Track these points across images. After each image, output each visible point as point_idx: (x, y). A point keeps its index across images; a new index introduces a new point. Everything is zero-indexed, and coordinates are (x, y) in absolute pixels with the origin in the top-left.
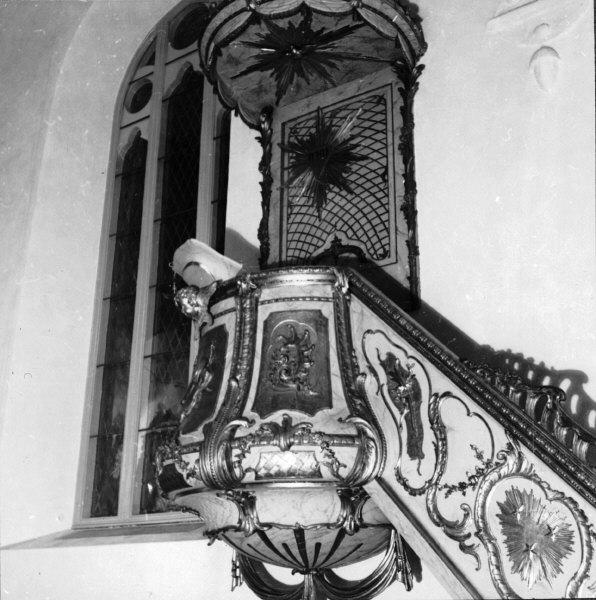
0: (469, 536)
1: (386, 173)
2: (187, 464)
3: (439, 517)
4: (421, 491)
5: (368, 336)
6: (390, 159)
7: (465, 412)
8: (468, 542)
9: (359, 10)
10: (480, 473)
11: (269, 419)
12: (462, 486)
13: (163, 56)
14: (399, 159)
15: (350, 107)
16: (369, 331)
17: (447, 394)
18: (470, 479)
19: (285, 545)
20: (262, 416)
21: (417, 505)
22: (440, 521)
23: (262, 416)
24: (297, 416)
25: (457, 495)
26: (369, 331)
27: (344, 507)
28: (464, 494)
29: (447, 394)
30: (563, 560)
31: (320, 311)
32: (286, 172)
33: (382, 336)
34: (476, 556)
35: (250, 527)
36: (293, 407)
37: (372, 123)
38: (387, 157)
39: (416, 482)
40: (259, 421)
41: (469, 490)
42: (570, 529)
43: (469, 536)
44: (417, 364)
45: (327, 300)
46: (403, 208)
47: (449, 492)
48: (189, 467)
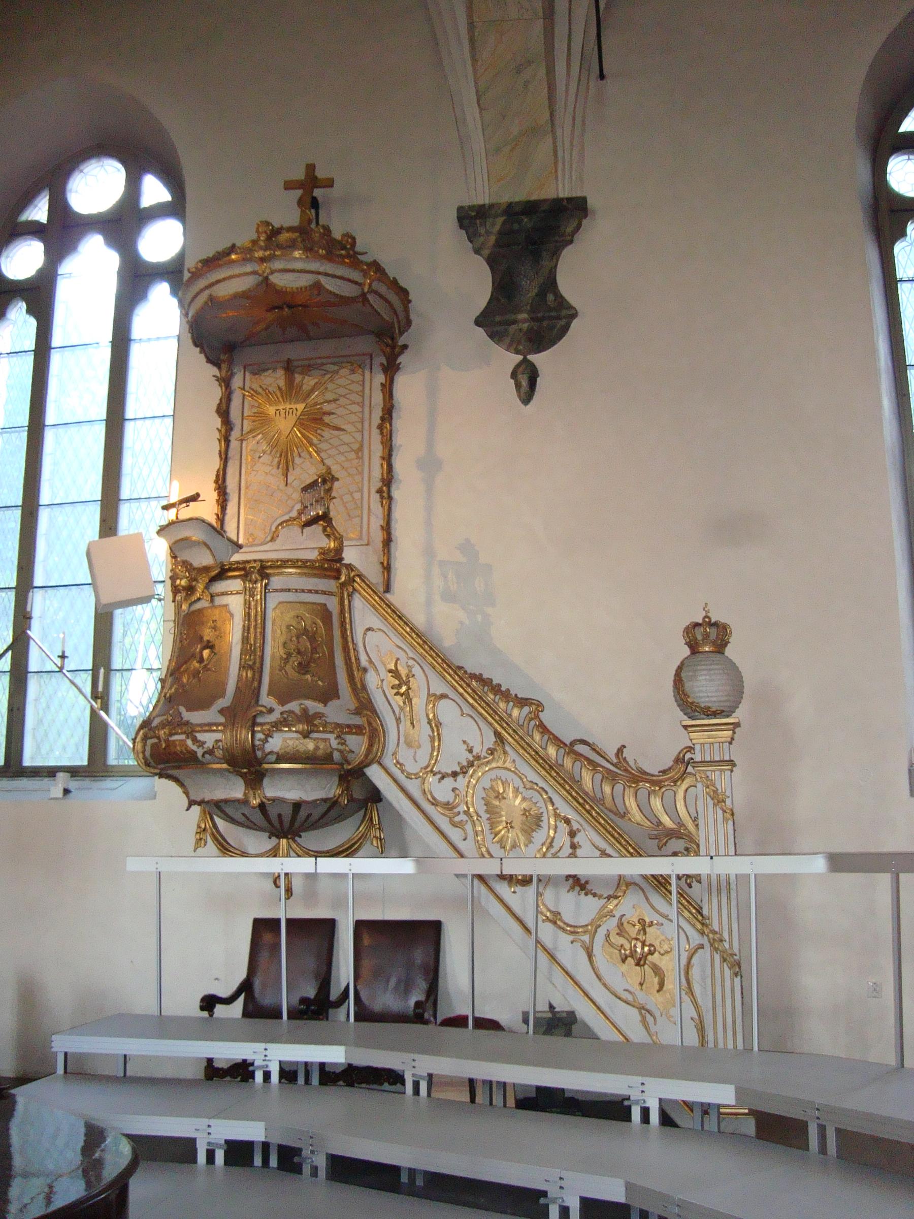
0: (459, 813)
1: (361, 449)
2: (204, 743)
3: (434, 798)
4: (417, 776)
5: (369, 633)
6: (366, 434)
7: (460, 713)
8: (457, 819)
9: (369, 296)
10: (471, 764)
11: (288, 707)
12: (455, 774)
13: (260, 397)
14: (376, 437)
15: (324, 367)
16: (369, 629)
17: (443, 696)
18: (461, 769)
19: (280, 816)
20: (282, 703)
21: (413, 787)
22: (435, 803)
23: (282, 703)
24: (313, 706)
25: (449, 781)
26: (369, 629)
27: (340, 784)
28: (456, 781)
29: (443, 696)
30: (534, 834)
31: (325, 605)
32: (245, 421)
33: (381, 633)
34: (464, 830)
35: (255, 802)
36: (307, 697)
37: (347, 391)
38: (362, 432)
39: (411, 768)
40: (279, 709)
41: (460, 778)
42: (541, 811)
43: (459, 813)
44: (416, 664)
45: (331, 594)
46: (380, 491)
47: (443, 778)
48: (206, 746)
